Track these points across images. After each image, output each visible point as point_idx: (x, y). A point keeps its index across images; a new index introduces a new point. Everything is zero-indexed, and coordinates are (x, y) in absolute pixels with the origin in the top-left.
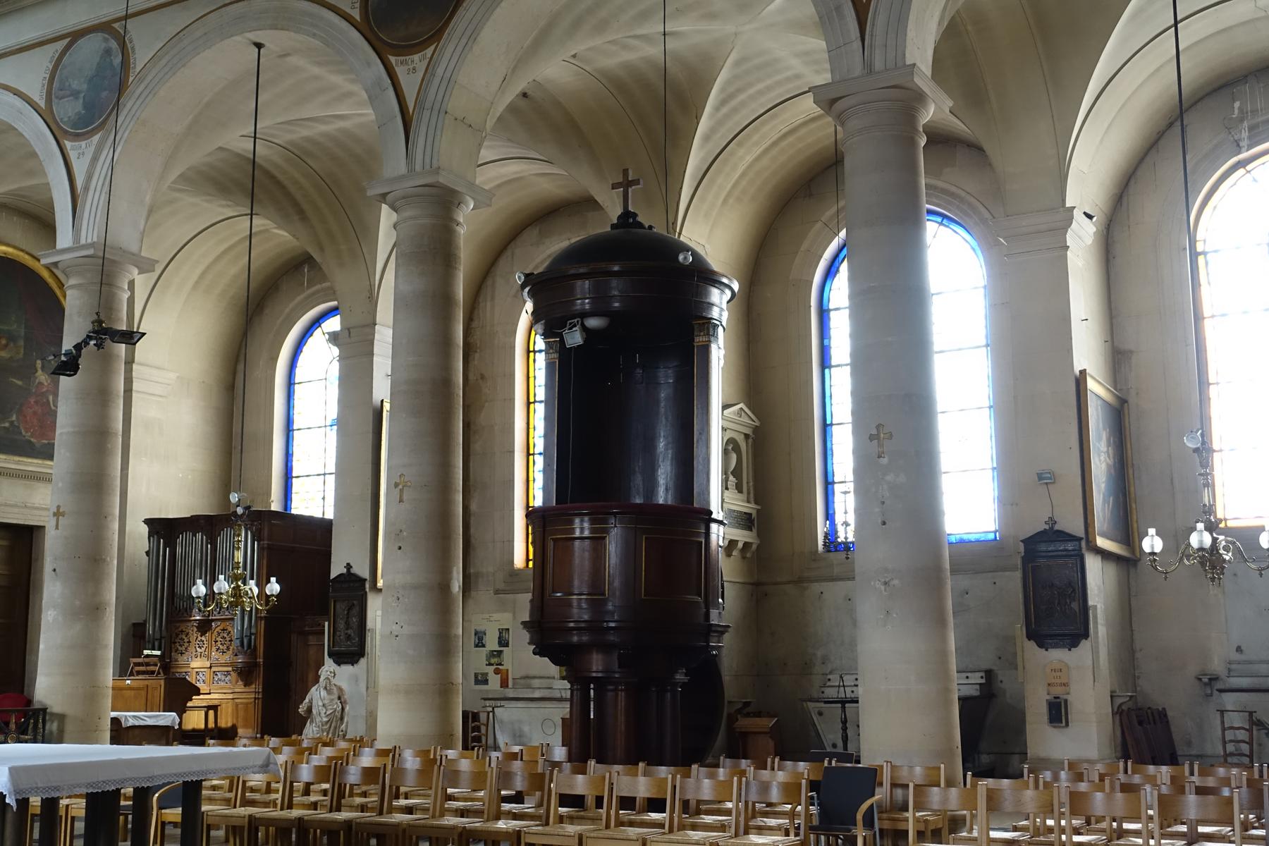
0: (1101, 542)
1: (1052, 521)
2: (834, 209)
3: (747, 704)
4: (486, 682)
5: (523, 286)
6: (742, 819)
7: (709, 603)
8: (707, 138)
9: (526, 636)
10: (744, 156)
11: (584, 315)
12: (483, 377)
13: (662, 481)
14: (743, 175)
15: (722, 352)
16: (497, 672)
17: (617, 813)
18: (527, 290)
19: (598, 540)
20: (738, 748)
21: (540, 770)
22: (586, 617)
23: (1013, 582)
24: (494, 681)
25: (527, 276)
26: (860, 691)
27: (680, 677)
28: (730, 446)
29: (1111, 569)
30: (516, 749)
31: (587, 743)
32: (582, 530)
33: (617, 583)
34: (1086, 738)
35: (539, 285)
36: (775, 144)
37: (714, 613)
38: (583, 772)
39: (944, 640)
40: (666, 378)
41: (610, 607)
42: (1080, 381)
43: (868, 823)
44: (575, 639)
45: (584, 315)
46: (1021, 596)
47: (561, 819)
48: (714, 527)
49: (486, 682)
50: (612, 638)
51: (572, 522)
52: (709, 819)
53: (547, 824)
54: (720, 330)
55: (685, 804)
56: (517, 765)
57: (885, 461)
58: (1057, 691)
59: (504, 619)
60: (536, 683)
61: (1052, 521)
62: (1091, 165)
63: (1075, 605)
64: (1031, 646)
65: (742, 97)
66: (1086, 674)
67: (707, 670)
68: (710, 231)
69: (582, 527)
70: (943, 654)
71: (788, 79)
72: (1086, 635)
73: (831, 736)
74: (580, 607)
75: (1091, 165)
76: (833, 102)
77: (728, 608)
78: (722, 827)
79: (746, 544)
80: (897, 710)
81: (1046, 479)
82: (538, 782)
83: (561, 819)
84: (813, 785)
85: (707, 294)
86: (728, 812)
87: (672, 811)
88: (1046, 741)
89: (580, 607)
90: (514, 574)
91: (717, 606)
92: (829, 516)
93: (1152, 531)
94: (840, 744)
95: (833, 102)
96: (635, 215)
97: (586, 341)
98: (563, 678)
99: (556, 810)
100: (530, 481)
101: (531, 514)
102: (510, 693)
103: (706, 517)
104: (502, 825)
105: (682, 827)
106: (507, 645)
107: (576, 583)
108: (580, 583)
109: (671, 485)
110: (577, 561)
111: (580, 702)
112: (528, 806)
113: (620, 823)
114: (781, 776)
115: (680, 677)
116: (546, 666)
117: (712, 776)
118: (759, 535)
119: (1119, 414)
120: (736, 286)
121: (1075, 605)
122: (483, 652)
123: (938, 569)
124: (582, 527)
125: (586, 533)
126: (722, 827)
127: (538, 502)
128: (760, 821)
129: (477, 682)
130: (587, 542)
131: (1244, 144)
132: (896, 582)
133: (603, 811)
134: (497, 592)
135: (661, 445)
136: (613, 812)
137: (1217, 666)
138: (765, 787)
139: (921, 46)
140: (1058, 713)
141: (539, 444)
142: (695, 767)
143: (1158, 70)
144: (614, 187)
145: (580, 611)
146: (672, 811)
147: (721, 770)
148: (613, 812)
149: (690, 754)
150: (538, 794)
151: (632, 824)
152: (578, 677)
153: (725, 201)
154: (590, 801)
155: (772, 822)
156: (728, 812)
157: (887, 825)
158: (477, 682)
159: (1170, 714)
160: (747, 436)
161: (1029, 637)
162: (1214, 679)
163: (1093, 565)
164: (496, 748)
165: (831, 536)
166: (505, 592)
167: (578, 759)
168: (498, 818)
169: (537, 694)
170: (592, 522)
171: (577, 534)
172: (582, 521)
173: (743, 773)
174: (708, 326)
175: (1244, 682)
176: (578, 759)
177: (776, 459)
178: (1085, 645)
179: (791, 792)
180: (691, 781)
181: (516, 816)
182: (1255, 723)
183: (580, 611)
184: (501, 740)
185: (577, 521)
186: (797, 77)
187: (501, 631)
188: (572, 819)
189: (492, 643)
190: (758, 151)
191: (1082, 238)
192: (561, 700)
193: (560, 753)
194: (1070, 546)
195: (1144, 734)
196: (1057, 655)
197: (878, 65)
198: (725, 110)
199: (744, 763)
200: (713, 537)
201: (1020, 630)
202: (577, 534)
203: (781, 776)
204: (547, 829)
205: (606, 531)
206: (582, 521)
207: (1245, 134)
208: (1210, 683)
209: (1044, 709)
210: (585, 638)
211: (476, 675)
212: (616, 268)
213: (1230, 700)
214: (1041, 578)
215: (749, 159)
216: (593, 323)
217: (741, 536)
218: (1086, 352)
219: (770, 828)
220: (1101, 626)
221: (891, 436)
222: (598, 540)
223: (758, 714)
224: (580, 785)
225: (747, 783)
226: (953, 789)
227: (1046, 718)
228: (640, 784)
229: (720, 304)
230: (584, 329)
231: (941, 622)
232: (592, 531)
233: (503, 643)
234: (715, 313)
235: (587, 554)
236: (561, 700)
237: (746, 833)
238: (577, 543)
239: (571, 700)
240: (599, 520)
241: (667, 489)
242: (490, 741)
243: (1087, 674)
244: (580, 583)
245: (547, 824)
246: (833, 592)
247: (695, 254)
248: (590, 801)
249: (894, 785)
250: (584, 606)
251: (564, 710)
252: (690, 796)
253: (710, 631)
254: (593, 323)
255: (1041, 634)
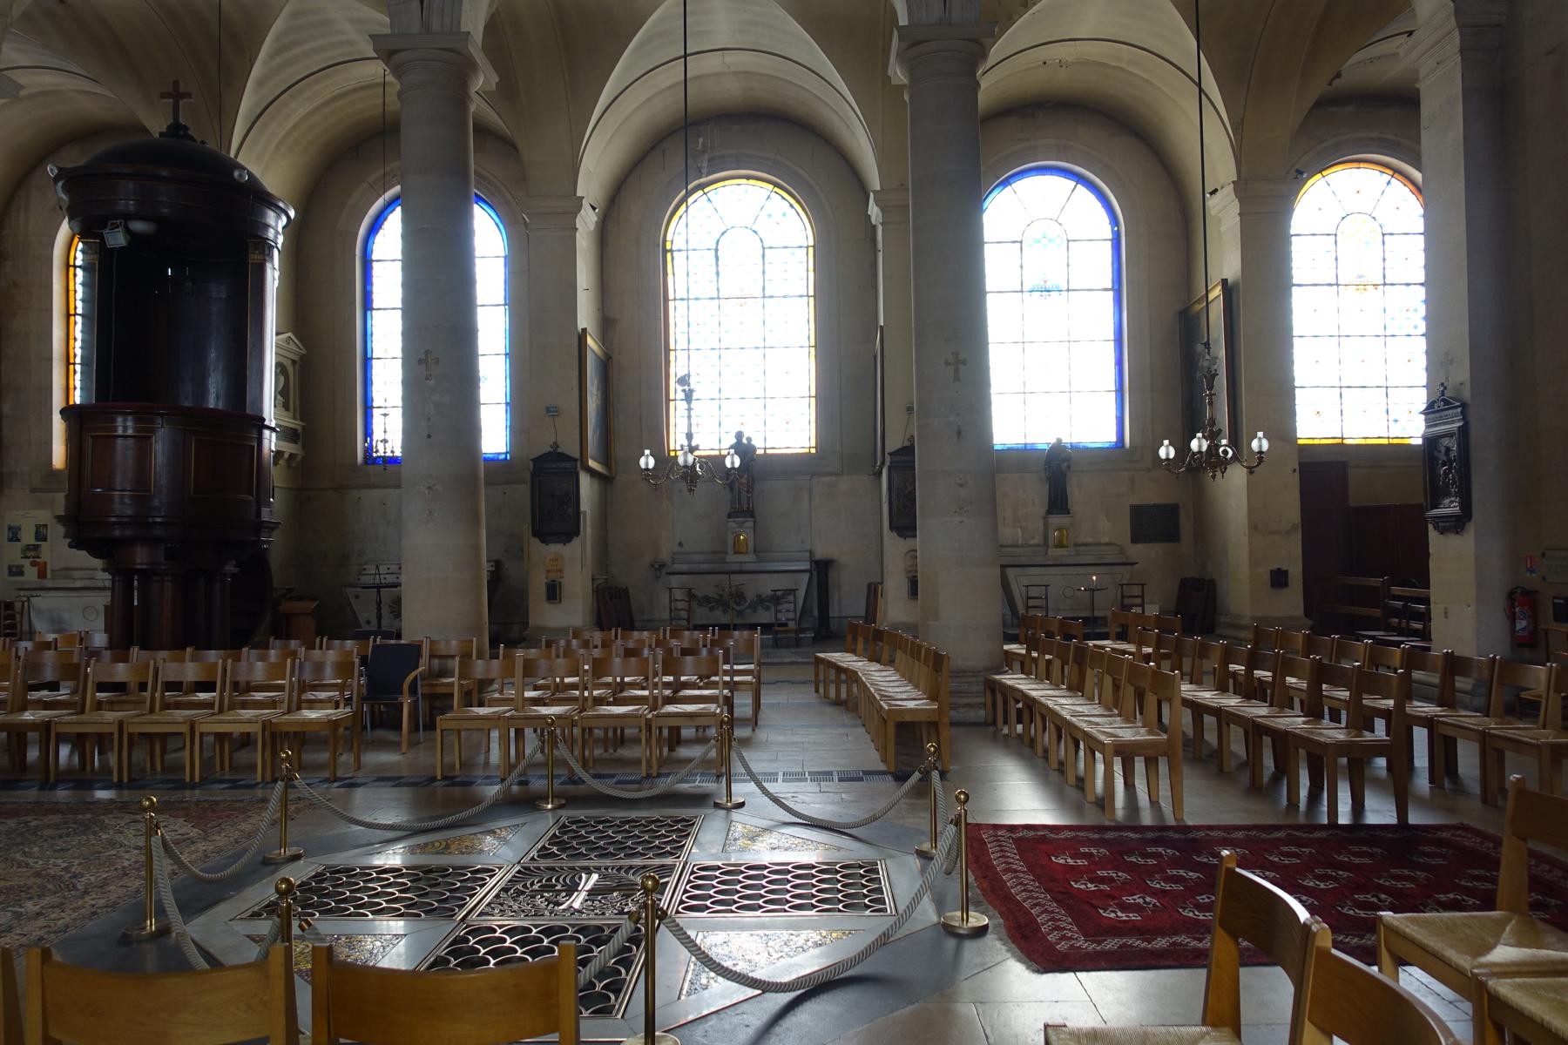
0: (592, 463)
1: (555, 445)
2: (381, 172)
3: (290, 590)
4: (21, 573)
5: (56, 179)
6: (295, 694)
7: (261, 502)
8: (261, 83)
9: (61, 530)
10: (297, 109)
11: (128, 217)
12: (15, 285)
13: (212, 390)
14: (295, 127)
15: (277, 274)
16: (33, 564)
17: (163, 696)
18: (60, 184)
19: (143, 440)
20: (283, 630)
21: (75, 660)
22: (129, 512)
23: (523, 492)
24: (31, 574)
25: (60, 169)
26: (403, 579)
27: (230, 568)
28: (281, 369)
29: (596, 483)
30: (50, 637)
31: (129, 630)
32: (125, 429)
33: (163, 481)
34: (574, 611)
35: (71, 179)
36: (327, 103)
37: (265, 512)
38: (125, 660)
39: (478, 537)
40: (218, 292)
41: (156, 503)
42: (874, 227)
43: (413, 690)
44: (117, 533)
45: (128, 217)
46: (528, 504)
47: (99, 706)
48: (267, 433)
49: (21, 573)
50: (159, 532)
51: (114, 421)
52: (259, 696)
53: (83, 712)
54: (276, 252)
55: (236, 686)
56: (49, 656)
57: (431, 383)
58: (553, 576)
59: (44, 516)
60: (78, 574)
61: (555, 445)
62: (594, 173)
63: (570, 511)
64: (535, 541)
65: (297, 51)
66: (575, 561)
67: (257, 563)
68: (267, 156)
69: (125, 426)
70: (477, 547)
71: (342, 43)
72: (577, 533)
73: (365, 613)
74: (122, 503)
75: (594, 173)
76: (393, 52)
77: (276, 508)
78: (272, 704)
79: (291, 455)
80: (434, 595)
81: (552, 412)
82: (72, 671)
83: (99, 706)
84: (364, 661)
85: (263, 215)
86: (280, 688)
87: (223, 689)
88: (547, 616)
89: (122, 503)
90: (53, 474)
91: (269, 505)
92: (368, 433)
93: (647, 452)
94: (374, 621)
95: (393, 52)
96: (186, 128)
97: (130, 243)
98: (104, 570)
99: (93, 696)
100: (69, 383)
101: (69, 412)
102: (49, 583)
103: (260, 423)
104: (28, 716)
105: (233, 707)
106: (45, 540)
107: (118, 479)
108: (123, 476)
109: (222, 393)
110: (119, 458)
111: (122, 590)
112: (63, 694)
113: (166, 706)
114: (331, 656)
115: (230, 568)
116: (82, 557)
117: (263, 658)
118: (304, 448)
119: (606, 364)
120: (292, 214)
121: (570, 511)
122: (18, 546)
123: (475, 477)
124: (125, 426)
125: (130, 432)
126: (272, 704)
127: (77, 398)
128: (309, 695)
129: (11, 573)
130: (131, 441)
131: (704, 171)
132: (439, 487)
133: (147, 694)
134: (33, 490)
135: (213, 355)
136: (157, 695)
137: (665, 556)
138: (319, 667)
139: (474, 20)
140: (554, 592)
141: (77, 349)
142: (245, 650)
143: (649, 99)
144: (163, 96)
145: (122, 505)
146: (223, 689)
147: (273, 652)
148: (157, 695)
149: (237, 639)
150: (70, 683)
151: (178, 706)
152: (122, 573)
153: (277, 148)
154: (133, 686)
155: (322, 695)
156: (280, 688)
157: (427, 690)
158: (11, 573)
159: (631, 591)
160: (294, 362)
161: (535, 534)
162: (663, 565)
163: (585, 480)
164: (31, 634)
165: (369, 450)
166: (41, 491)
167: (121, 644)
168: (24, 709)
169: (78, 584)
170: (136, 421)
171: (120, 432)
172: (125, 421)
173: (294, 654)
174: (265, 247)
175: (684, 567)
176: (121, 644)
177: (325, 375)
178: (576, 541)
179: (344, 669)
180: (243, 664)
181: (47, 705)
182: (691, 596)
183: (122, 505)
184: (39, 625)
185: (120, 419)
186: (351, 43)
187: (38, 527)
188: (111, 706)
189: (28, 537)
190: (309, 107)
191: (587, 221)
192: (103, 589)
193: (100, 639)
194: (568, 465)
195: (614, 609)
196: (555, 548)
197: (435, 26)
198: (279, 60)
199: (293, 644)
200: (266, 442)
201: (527, 529)
202: (120, 432)
203: (331, 656)
204: (83, 717)
205: (153, 431)
206: (125, 421)
207: (705, 164)
208: (659, 568)
209: (543, 590)
210: (128, 533)
211: (10, 568)
212: (165, 173)
213: (675, 581)
214: (543, 486)
215: (301, 112)
216: (138, 226)
217: (288, 448)
218: (585, 317)
219: (321, 701)
220: (588, 527)
221: (438, 361)
222: (143, 440)
223: (300, 598)
224: (121, 672)
225: (301, 664)
226: (495, 661)
227: (544, 596)
228: (190, 671)
229: (276, 226)
230: (128, 231)
231: (476, 521)
232: (136, 429)
233: (41, 535)
234: (271, 234)
235: (130, 452)
236: (103, 589)
237: (299, 708)
238: (119, 441)
239: (113, 589)
240: (145, 421)
241: (218, 397)
242: (26, 627)
243: (575, 561)
244: (123, 476)
245: (83, 712)
246: (371, 498)
247: (250, 174)
248: (133, 686)
249: (432, 656)
250: (127, 501)
251: (104, 599)
252: (242, 678)
253: (260, 526)
254: (138, 226)
255: (545, 532)
